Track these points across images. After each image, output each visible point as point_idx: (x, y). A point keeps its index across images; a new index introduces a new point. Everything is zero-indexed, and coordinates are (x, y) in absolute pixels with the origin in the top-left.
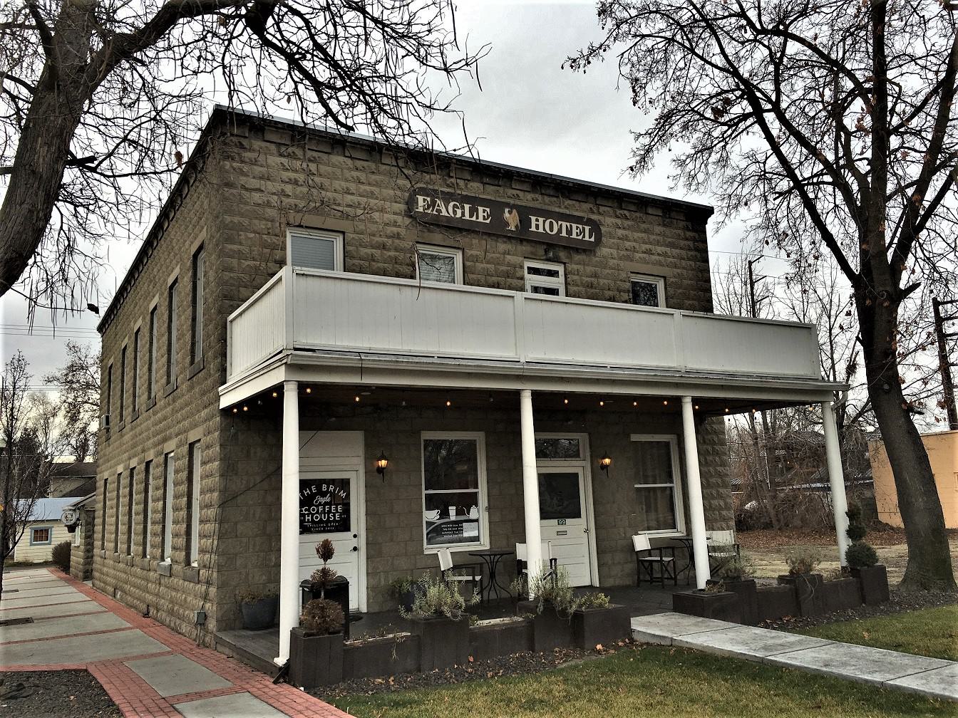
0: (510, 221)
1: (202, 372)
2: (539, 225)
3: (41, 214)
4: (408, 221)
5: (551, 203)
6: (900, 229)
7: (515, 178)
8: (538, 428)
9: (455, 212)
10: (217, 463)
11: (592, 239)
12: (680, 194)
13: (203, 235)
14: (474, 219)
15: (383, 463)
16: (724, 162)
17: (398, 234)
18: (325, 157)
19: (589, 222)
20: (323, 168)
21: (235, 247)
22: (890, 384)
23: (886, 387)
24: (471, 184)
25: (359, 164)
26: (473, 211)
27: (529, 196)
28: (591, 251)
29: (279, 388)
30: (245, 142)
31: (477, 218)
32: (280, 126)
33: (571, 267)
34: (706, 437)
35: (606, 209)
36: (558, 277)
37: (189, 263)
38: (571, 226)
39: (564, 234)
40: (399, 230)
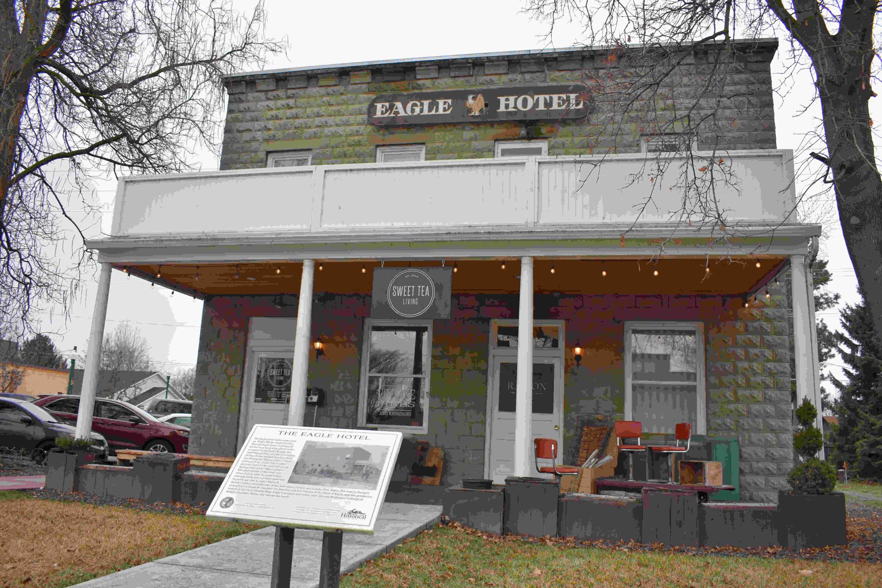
2: (507, 104)
4: (370, 128)
7: (486, 63)
9: (413, 111)
14: (433, 112)
18: (301, 92)
24: (438, 81)
25: (330, 90)
27: (505, 78)
30: (243, 97)
32: (265, 77)
34: (749, 324)
40: (360, 137)
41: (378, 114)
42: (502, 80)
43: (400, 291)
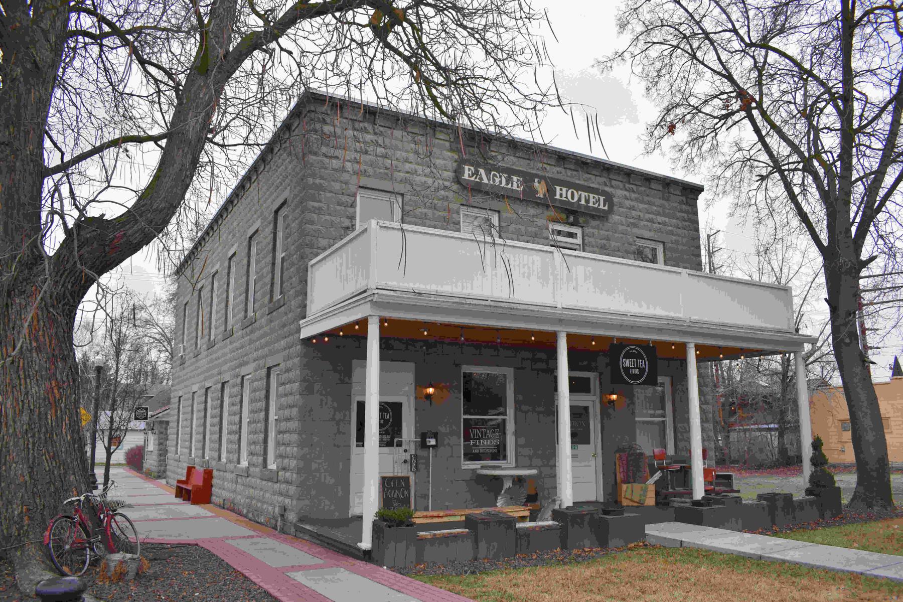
0: (539, 189)
1: (283, 308)
2: (561, 193)
3: (188, 173)
4: (455, 187)
5: (572, 176)
6: (860, 213)
8: (572, 366)
10: (297, 384)
11: (606, 208)
12: (679, 175)
13: (286, 194)
14: (509, 186)
15: (431, 390)
16: (714, 148)
17: (447, 197)
18: (389, 132)
19: (603, 193)
20: (387, 141)
21: (316, 204)
22: (851, 339)
23: (847, 341)
26: (509, 180)
28: (603, 217)
29: (363, 323)
31: (512, 186)
33: (588, 230)
35: (617, 183)
36: (576, 238)
37: (271, 217)
38: (589, 196)
39: (583, 202)
41: (466, 176)
42: (553, 171)
43: (627, 363)
